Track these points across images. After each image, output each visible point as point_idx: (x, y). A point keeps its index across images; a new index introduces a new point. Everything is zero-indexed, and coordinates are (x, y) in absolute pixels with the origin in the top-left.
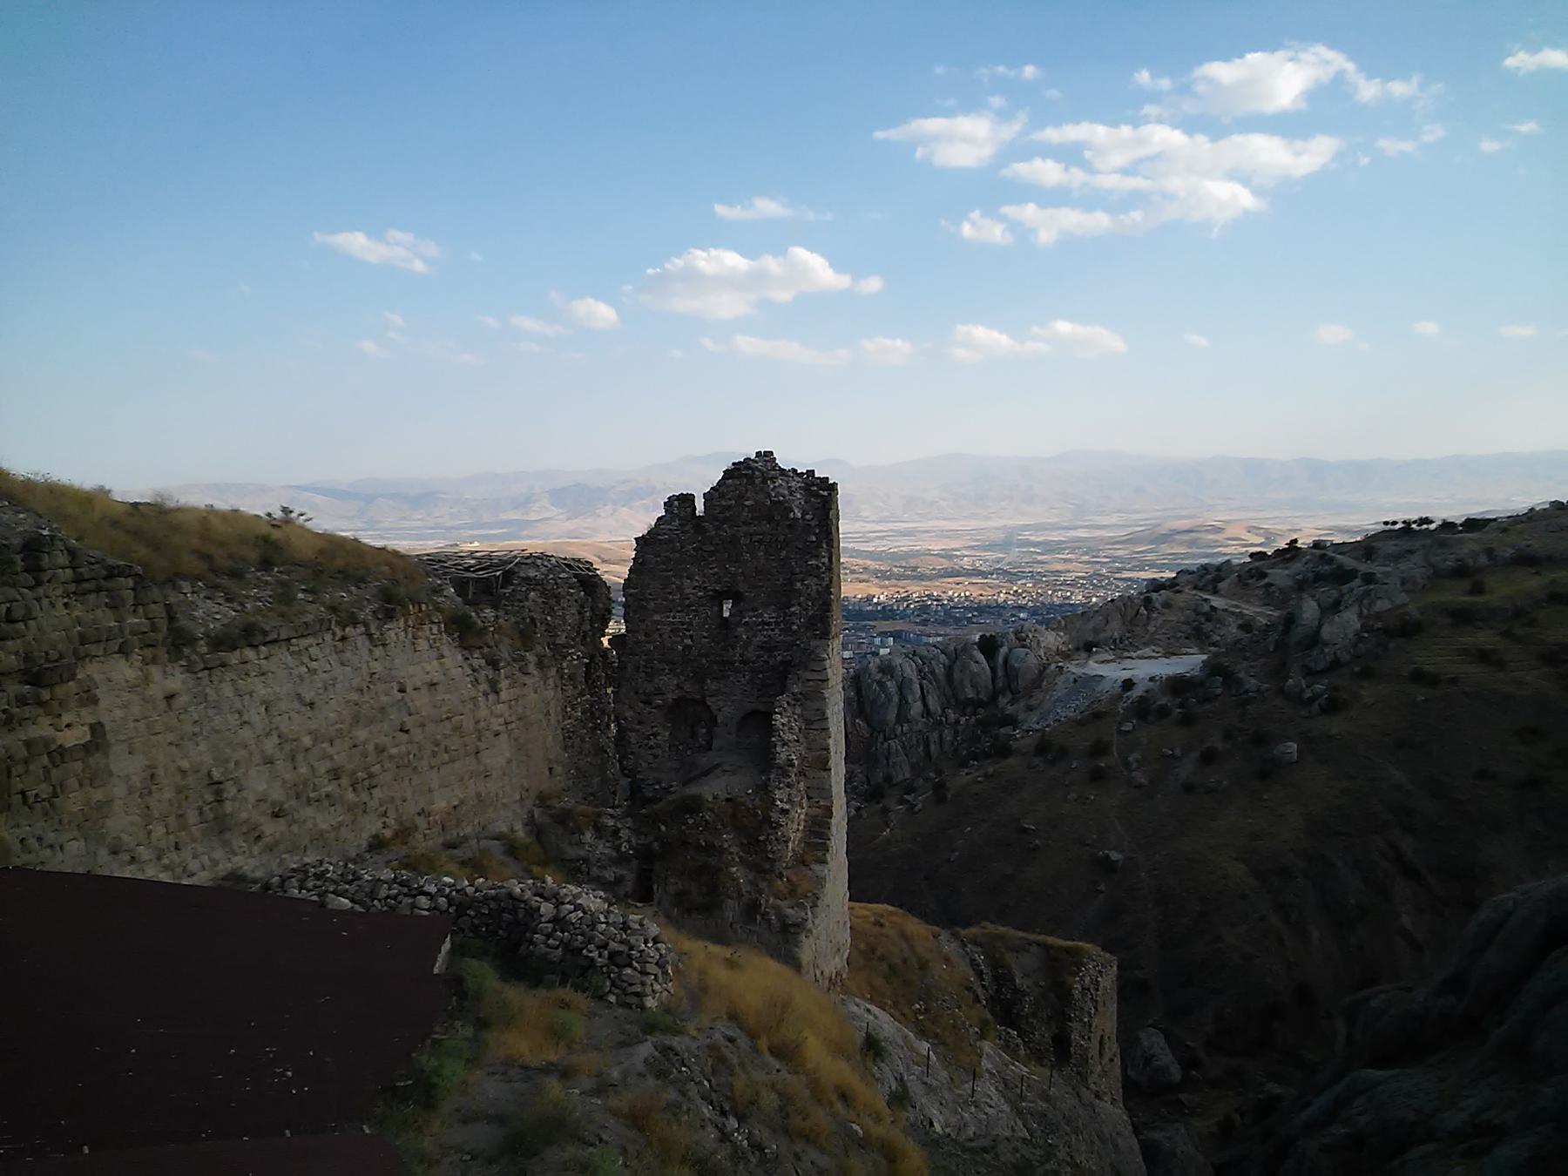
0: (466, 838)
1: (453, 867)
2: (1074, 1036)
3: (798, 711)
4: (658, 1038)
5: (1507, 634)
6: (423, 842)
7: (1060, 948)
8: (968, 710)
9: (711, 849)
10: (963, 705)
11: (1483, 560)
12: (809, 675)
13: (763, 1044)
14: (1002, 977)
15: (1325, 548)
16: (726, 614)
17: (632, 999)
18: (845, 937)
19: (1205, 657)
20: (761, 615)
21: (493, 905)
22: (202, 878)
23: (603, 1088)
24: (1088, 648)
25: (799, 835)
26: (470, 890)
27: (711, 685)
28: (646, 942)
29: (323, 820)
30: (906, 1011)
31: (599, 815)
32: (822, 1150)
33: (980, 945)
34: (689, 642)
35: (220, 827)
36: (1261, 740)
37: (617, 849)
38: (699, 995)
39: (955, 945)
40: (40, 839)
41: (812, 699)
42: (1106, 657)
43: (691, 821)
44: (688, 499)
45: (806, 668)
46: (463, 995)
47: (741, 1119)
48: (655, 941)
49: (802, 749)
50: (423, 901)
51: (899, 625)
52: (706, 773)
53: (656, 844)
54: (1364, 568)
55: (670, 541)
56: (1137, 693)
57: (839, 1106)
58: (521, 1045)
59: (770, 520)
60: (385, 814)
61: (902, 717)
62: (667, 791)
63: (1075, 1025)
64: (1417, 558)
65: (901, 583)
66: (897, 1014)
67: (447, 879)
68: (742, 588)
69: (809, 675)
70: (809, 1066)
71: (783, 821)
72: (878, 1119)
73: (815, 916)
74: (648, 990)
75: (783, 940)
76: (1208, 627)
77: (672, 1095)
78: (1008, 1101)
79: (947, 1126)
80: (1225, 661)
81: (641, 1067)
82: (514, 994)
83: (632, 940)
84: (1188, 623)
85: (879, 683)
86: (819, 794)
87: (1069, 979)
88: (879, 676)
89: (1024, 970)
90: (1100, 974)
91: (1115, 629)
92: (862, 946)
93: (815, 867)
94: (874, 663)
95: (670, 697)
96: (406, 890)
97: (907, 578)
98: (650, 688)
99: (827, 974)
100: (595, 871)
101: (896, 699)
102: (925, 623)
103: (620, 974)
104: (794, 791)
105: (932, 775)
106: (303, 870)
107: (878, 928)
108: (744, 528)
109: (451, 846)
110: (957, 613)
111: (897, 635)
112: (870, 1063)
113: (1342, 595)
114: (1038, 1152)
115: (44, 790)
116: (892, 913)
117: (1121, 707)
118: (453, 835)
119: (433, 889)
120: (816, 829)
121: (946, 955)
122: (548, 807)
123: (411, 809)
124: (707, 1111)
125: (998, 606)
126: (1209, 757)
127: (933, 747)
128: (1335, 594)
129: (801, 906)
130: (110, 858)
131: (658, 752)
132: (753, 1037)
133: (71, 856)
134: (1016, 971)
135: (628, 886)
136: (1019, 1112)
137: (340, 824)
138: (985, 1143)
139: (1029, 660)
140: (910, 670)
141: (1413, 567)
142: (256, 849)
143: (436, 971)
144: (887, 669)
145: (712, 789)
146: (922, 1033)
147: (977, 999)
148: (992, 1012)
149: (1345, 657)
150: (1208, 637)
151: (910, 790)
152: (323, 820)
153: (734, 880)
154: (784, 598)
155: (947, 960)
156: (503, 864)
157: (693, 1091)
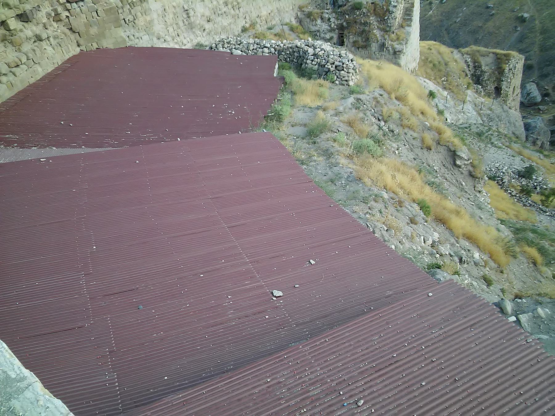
0: (274, 25)
1: (272, 37)
6: (260, 28)
7: (501, 54)
13: (393, 96)
14: (477, 66)
17: (345, 82)
21: (291, 50)
22: (189, 46)
23: (337, 114)
26: (282, 45)
28: (348, 61)
29: (225, 22)
31: (322, 13)
32: (414, 131)
33: (469, 54)
35: (191, 27)
37: (330, 26)
38: (368, 80)
40: (134, 36)
43: (358, 13)
46: (285, 84)
47: (385, 122)
50: (266, 50)
53: (345, 23)
57: (421, 116)
58: (307, 100)
60: (245, 18)
66: (435, 82)
67: (273, 41)
70: (410, 103)
71: (394, 10)
73: (406, 48)
74: (350, 79)
77: (361, 115)
78: (476, 111)
79: (452, 120)
81: (350, 106)
82: (303, 82)
89: (487, 64)
90: (517, 62)
92: (423, 58)
93: (407, 28)
96: (259, 46)
99: (410, 69)
100: (322, 35)
103: (340, 74)
106: (222, 41)
107: (429, 51)
109: (270, 29)
114: (486, 128)
115: (130, 18)
116: (435, 44)
118: (270, 25)
119: (269, 46)
121: (456, 59)
122: (303, 11)
123: (254, 15)
124: (374, 120)
129: (401, 44)
130: (158, 41)
132: (389, 93)
133: (145, 42)
134: (483, 63)
135: (335, 40)
136: (480, 115)
137: (231, 23)
138: (467, 125)
142: (204, 34)
143: (275, 75)
146: (445, 88)
147: (467, 75)
148: (472, 80)
152: (225, 22)
155: (456, 61)
156: (289, 34)
157: (368, 113)
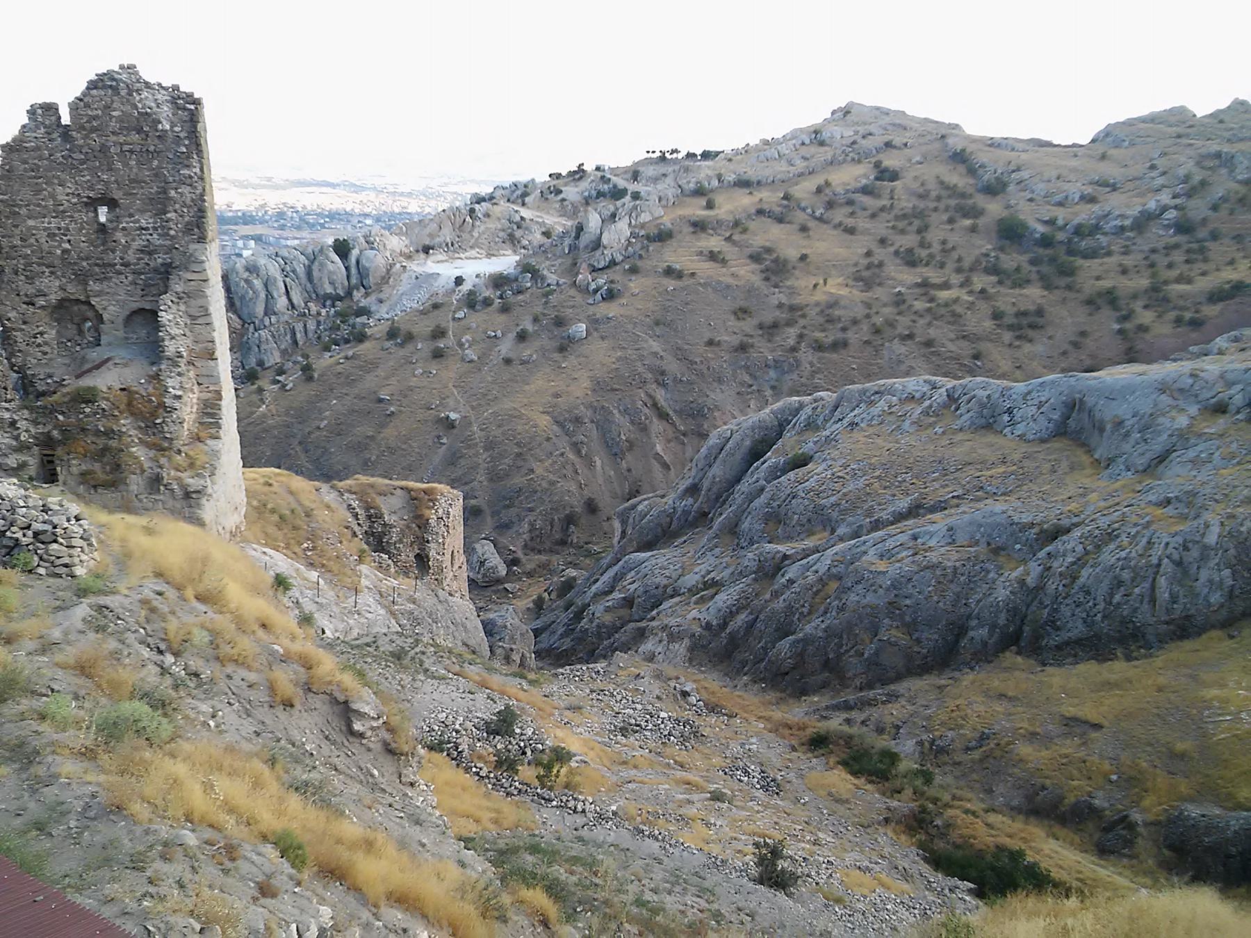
2: (432, 553)
3: (183, 307)
4: (92, 599)
5: (728, 239)
8: (328, 303)
9: (109, 433)
10: (323, 299)
11: (715, 183)
12: (189, 276)
13: (189, 593)
14: (374, 516)
16: (103, 219)
18: (242, 498)
19: (518, 258)
20: (138, 221)
23: (47, 647)
24: (426, 250)
25: (193, 416)
27: (94, 286)
28: (68, 521)
30: (297, 549)
32: (249, 668)
34: (67, 246)
36: (560, 322)
37: (17, 438)
38: (124, 560)
39: (334, 494)
41: (195, 295)
42: (440, 257)
44: (50, 109)
45: (187, 269)
47: (176, 654)
48: (77, 519)
49: (189, 342)
51: (259, 230)
52: (98, 367)
54: (632, 187)
55: (38, 148)
56: (466, 287)
57: (261, 633)
59: (139, 131)
61: (269, 311)
62: (60, 384)
63: (432, 545)
64: (669, 180)
65: (259, 192)
68: (117, 195)
69: (189, 276)
71: (177, 405)
72: (293, 638)
73: (213, 483)
74: (76, 560)
75: (188, 503)
76: (518, 233)
77: (112, 644)
80: (533, 261)
81: (80, 626)
83: (55, 520)
85: (247, 281)
86: (207, 380)
87: (427, 512)
88: (246, 275)
89: (392, 510)
90: (450, 504)
91: (447, 235)
94: (240, 264)
95: (53, 298)
97: (264, 187)
98: (31, 291)
99: (228, 529)
101: (263, 295)
102: (282, 227)
103: (47, 550)
104: (184, 379)
105: (300, 359)
107: (267, 488)
108: (114, 138)
110: (311, 219)
111: (258, 239)
112: (279, 595)
113: (617, 209)
114: (410, 640)
116: (279, 474)
120: (209, 410)
121: (328, 504)
124: (146, 653)
125: (346, 213)
126: (522, 337)
127: (298, 336)
128: (612, 208)
131: (46, 349)
132: (179, 588)
135: (32, 470)
136: (392, 613)
138: (369, 640)
139: (376, 261)
140: (274, 270)
141: (667, 188)
144: (252, 269)
145: (106, 381)
147: (355, 535)
148: (367, 543)
149: (619, 258)
151: (281, 372)
153: (136, 458)
154: (160, 205)
155: (328, 507)
157: (130, 637)
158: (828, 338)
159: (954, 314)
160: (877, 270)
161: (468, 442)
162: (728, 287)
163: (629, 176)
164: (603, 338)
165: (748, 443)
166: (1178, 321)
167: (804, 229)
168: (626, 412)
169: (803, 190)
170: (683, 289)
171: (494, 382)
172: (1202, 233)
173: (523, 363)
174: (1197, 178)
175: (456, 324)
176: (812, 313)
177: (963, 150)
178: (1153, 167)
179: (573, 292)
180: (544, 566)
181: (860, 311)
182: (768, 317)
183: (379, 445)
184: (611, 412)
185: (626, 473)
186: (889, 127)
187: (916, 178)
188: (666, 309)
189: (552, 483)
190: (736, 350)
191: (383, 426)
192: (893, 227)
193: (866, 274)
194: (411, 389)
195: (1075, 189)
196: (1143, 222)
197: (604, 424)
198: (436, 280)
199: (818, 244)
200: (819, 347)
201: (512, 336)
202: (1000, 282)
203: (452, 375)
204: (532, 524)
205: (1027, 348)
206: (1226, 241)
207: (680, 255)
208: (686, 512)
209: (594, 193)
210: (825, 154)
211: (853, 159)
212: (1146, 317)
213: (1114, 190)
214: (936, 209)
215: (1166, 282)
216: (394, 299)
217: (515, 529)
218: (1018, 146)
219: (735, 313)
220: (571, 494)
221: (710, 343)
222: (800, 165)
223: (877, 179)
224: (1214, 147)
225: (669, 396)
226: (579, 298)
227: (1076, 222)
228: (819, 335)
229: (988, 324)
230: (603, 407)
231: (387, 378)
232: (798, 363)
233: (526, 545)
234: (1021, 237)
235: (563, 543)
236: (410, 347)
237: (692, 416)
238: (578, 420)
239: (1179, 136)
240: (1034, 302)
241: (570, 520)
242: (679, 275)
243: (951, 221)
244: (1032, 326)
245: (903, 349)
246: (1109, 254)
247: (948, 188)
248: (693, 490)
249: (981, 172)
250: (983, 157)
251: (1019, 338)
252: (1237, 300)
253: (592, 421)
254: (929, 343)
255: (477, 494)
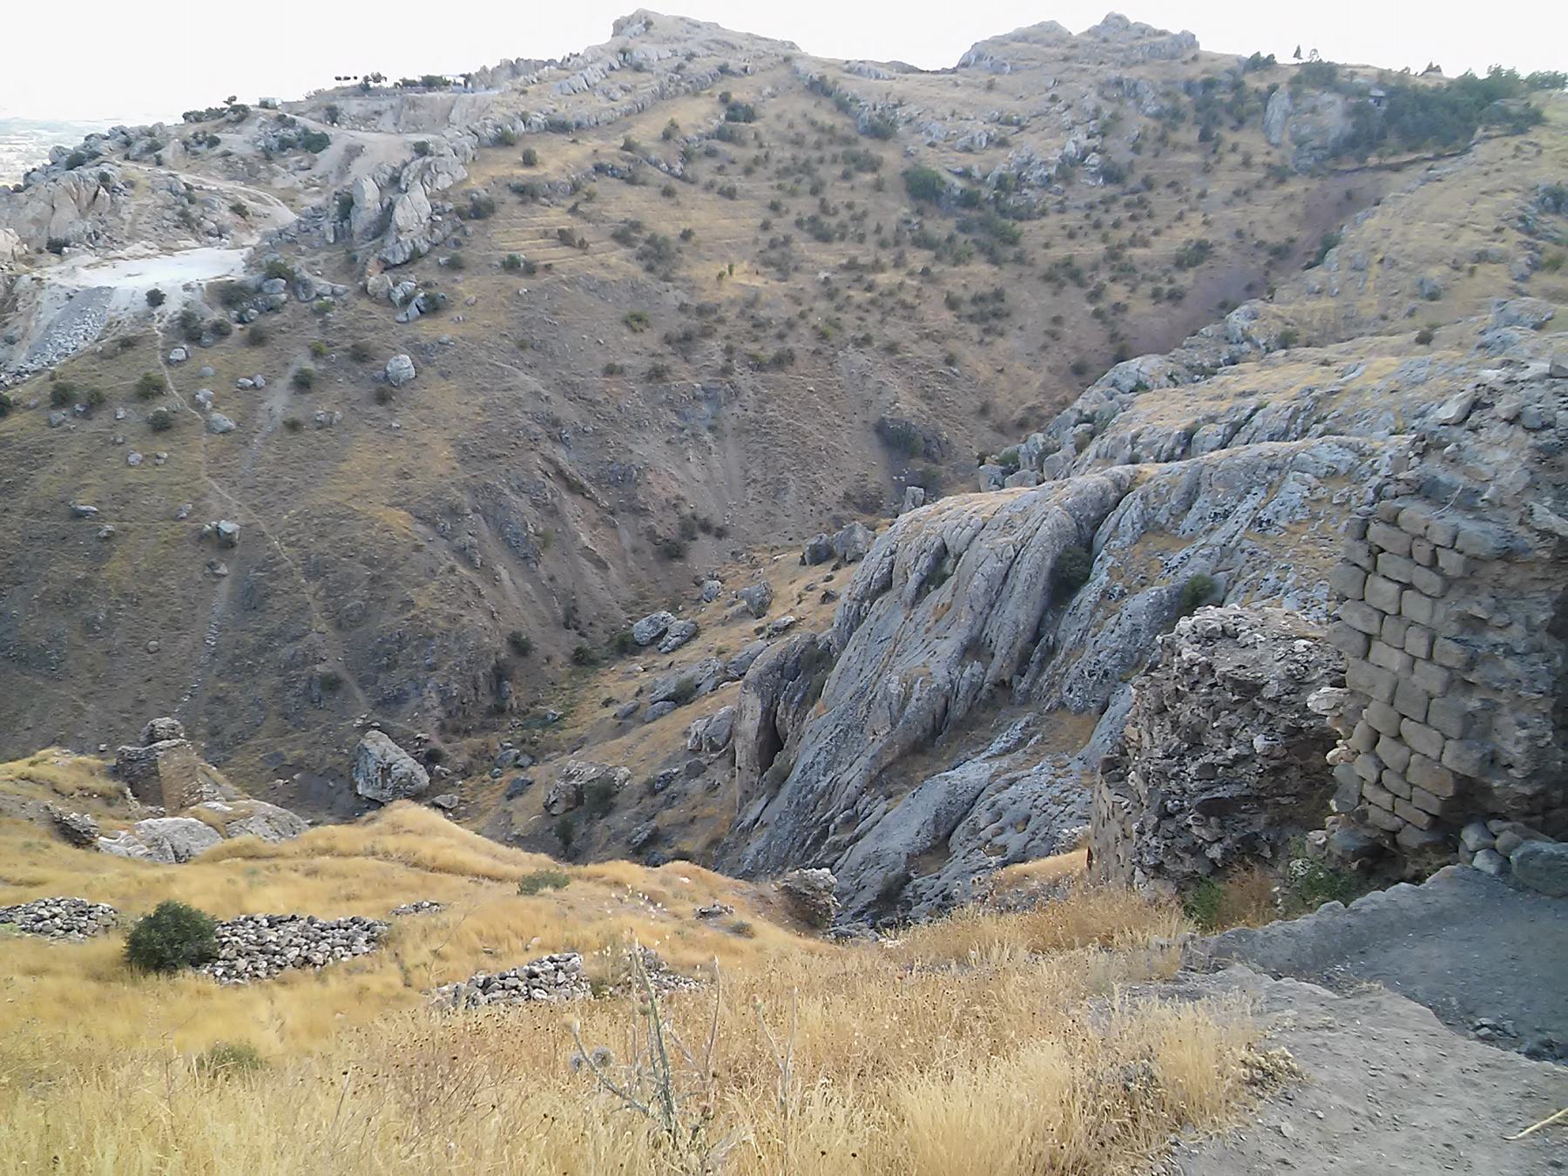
5: (573, 210)
11: (520, 126)
15: (275, 107)
36: (360, 355)
76: (194, 211)
84: (169, 208)
117: (157, 327)
126: (303, 383)
149: (424, 247)
150: (199, 225)
158: (770, 351)
159: (904, 305)
160: (784, 249)
161: (269, 565)
162: (603, 283)
163: (320, 114)
164: (445, 375)
165: (1048, 563)
166: (1156, 295)
167: (668, 193)
168: (520, 490)
169: (646, 132)
170: (542, 290)
171: (281, 461)
172: (1134, 181)
173: (321, 426)
174: (1107, 112)
175: (176, 371)
176: (731, 315)
177: (823, 78)
178: (1054, 99)
179: (364, 304)
180: (479, 755)
181: (788, 311)
182: (677, 324)
183: (107, 592)
184: (501, 494)
185: (549, 585)
186: (713, 45)
187: (779, 117)
188: (526, 323)
189: (453, 619)
190: (649, 378)
191: (99, 558)
192: (780, 187)
193: (774, 255)
194: (130, 488)
195: (979, 129)
196: (1068, 168)
197: (495, 515)
198: (108, 297)
199: (695, 214)
200: (758, 365)
201: (284, 382)
202: (938, 258)
203: (199, 457)
204: (443, 692)
205: (1001, 344)
206: (1162, 190)
207: (518, 234)
208: (976, 687)
209: (274, 143)
210: (647, 85)
211: (687, 91)
212: (1118, 292)
213: (1022, 129)
214: (821, 161)
215: (1121, 246)
216: (36, 335)
217: (414, 702)
218: (884, 72)
219: (626, 322)
220: (485, 630)
221: (610, 370)
222: (624, 101)
223: (728, 118)
224: (1114, 74)
225: (573, 456)
226: (379, 313)
227: (996, 173)
228: (753, 347)
229: (948, 316)
230: (486, 486)
231: (79, 474)
232: (736, 392)
233: (443, 727)
234: (938, 194)
235: (499, 710)
236: (100, 421)
237: (615, 483)
238: (454, 512)
239: (1066, 59)
240: (986, 283)
241: (500, 674)
242: (530, 270)
243: (846, 176)
244: (996, 315)
245: (862, 359)
246: (1044, 213)
247: (822, 130)
248: (975, 648)
249: (854, 107)
250: (851, 87)
251: (987, 331)
252: (1206, 264)
253: (475, 511)
254: (891, 349)
255: (322, 654)
